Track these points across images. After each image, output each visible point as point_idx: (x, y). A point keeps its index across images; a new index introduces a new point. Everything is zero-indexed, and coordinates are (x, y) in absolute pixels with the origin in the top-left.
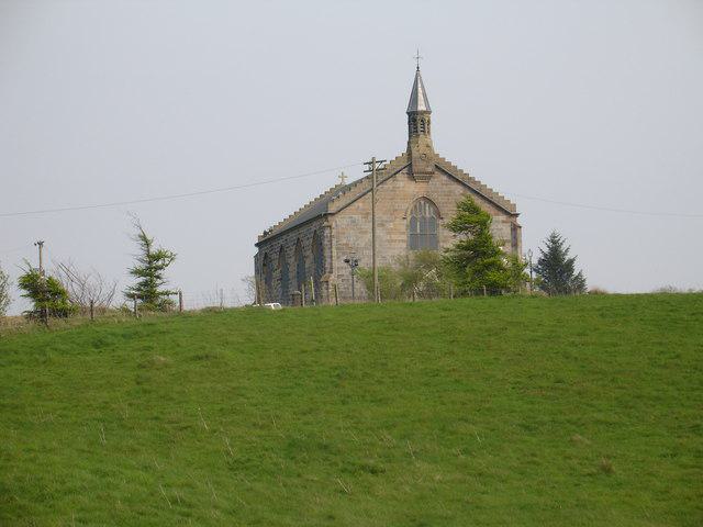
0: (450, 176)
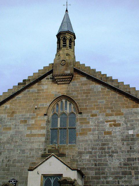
0: (89, 77)
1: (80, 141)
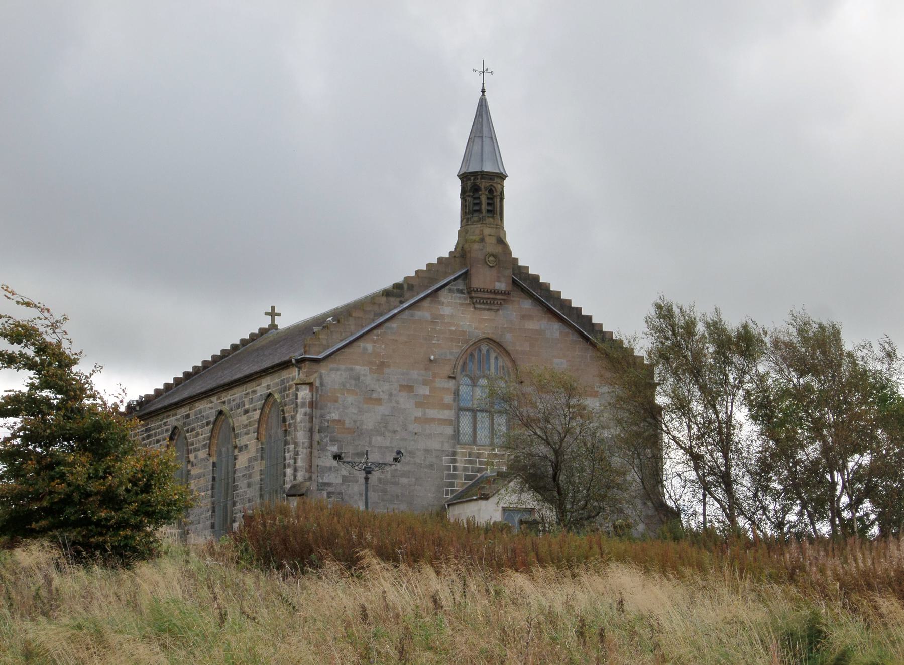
1: (865, 566)
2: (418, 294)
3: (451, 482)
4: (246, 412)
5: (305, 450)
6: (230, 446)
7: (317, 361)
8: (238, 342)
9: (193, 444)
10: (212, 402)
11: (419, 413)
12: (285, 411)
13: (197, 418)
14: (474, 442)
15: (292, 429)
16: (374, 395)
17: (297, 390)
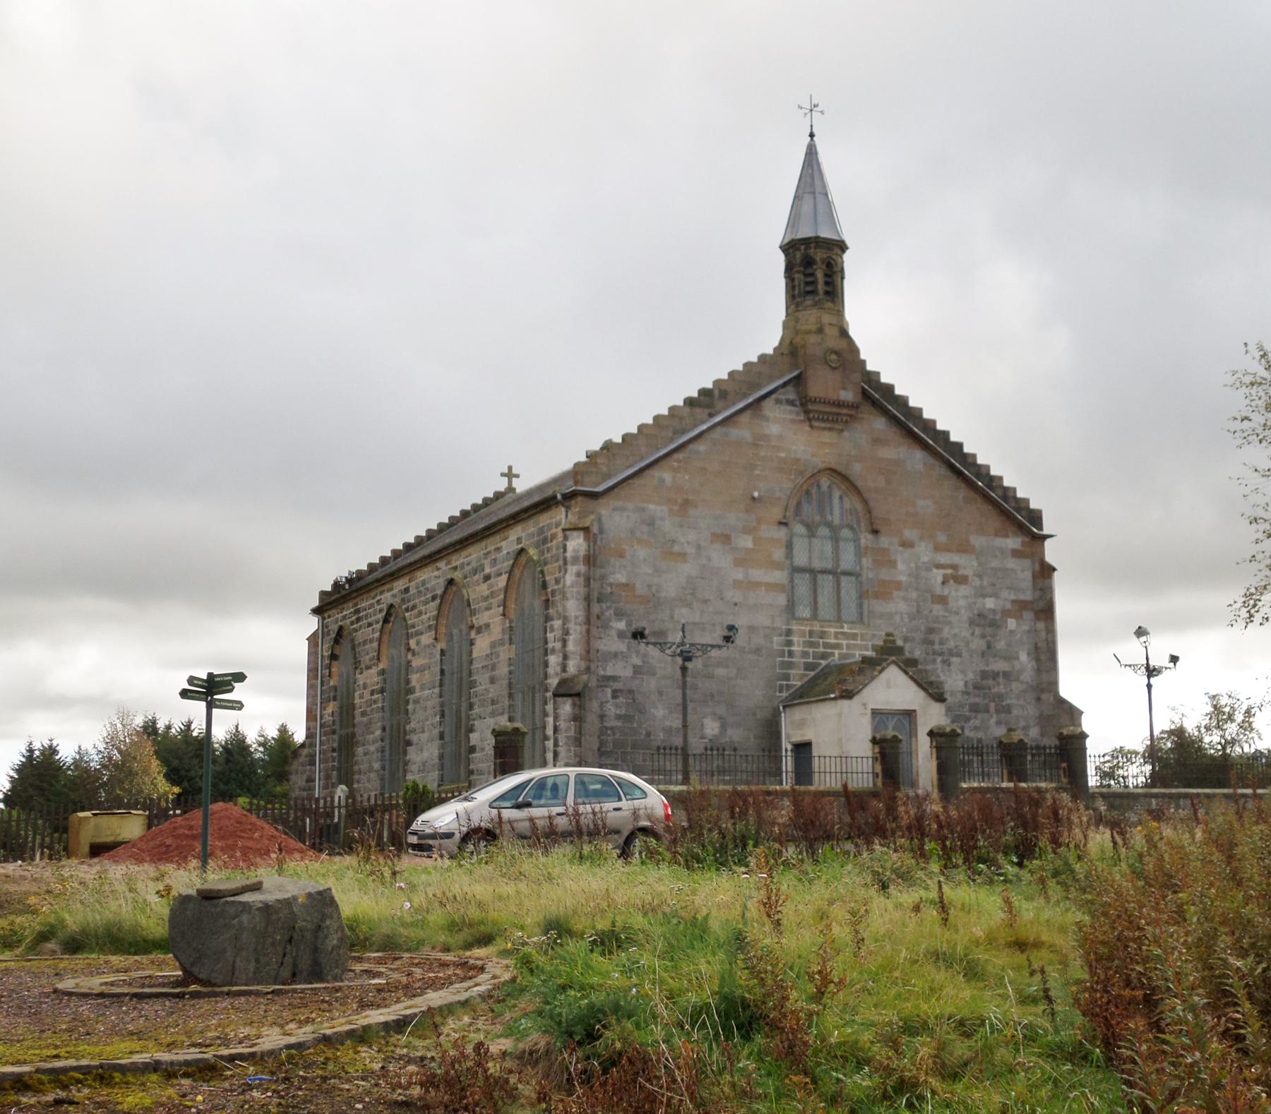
2: (734, 404)
3: (784, 674)
4: (487, 578)
5: (578, 628)
6: (464, 627)
7: (593, 496)
8: (469, 508)
9: (413, 626)
10: (438, 569)
11: (739, 575)
12: (546, 573)
13: (420, 592)
14: (815, 616)
15: (558, 597)
16: (676, 548)
17: (566, 538)
